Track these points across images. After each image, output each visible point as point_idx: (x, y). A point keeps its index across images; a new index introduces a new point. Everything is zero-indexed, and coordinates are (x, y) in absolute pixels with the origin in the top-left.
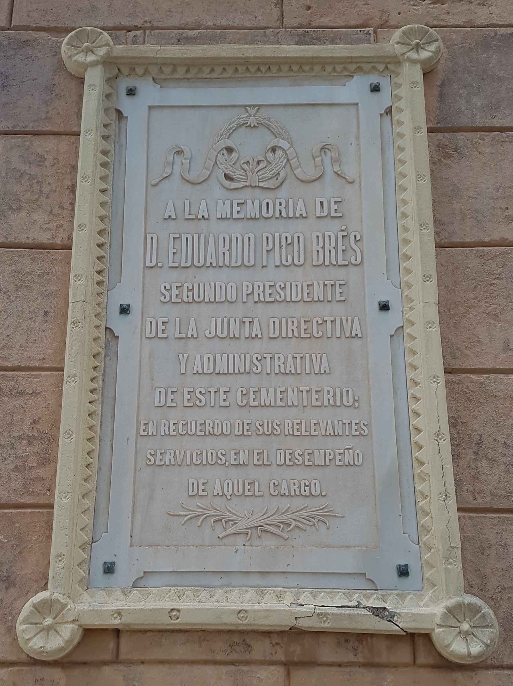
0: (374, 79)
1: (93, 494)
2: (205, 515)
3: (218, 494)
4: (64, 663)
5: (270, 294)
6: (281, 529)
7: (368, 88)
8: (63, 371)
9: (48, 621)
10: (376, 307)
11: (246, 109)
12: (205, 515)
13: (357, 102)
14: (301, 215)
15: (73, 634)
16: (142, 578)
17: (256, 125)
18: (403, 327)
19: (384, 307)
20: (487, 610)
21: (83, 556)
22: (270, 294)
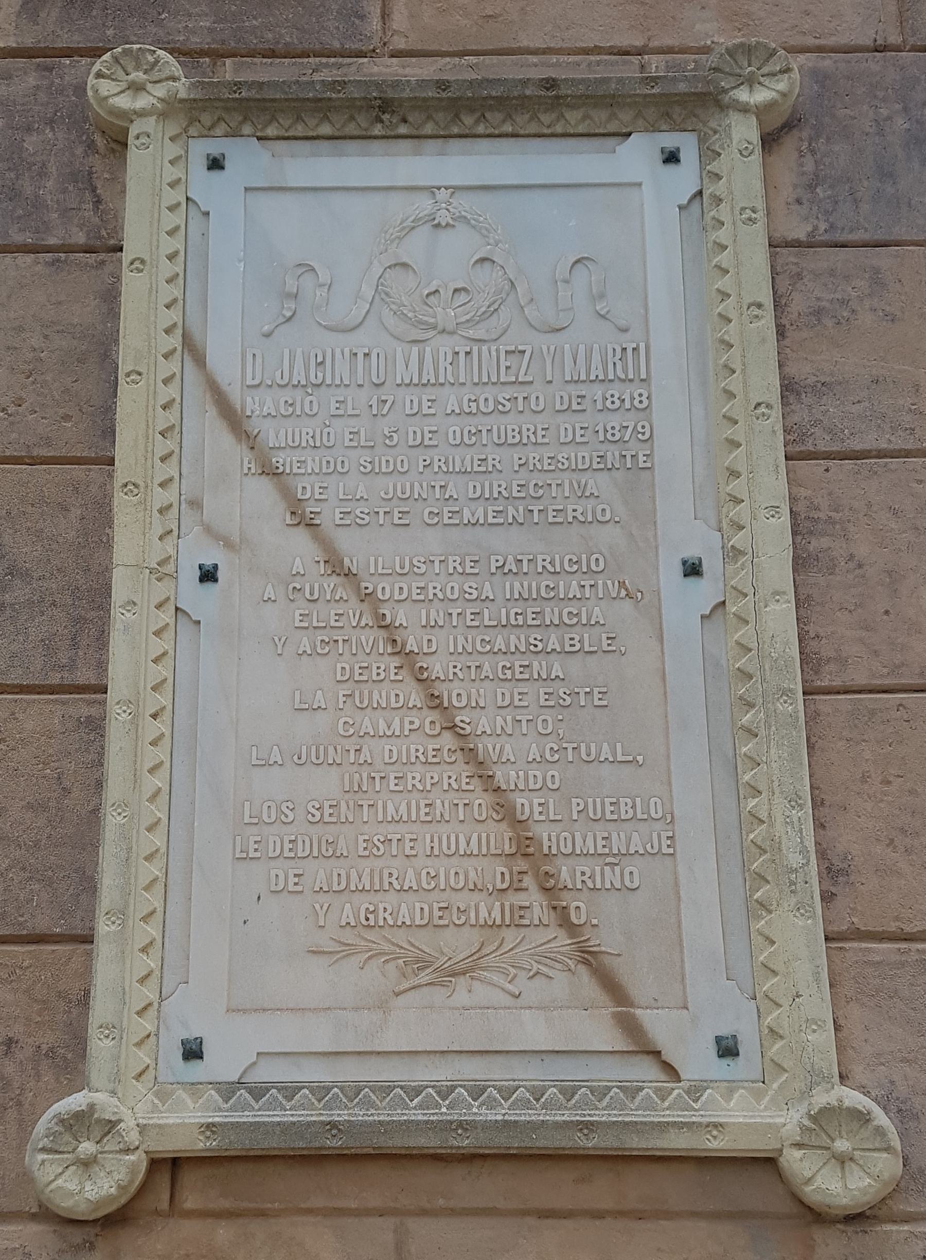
0: (670, 140)
1: (167, 740)
2: (370, 954)
3: (453, 411)
4: (116, 1219)
5: (507, 368)
6: (510, 977)
7: (658, 157)
8: (106, 693)
9: (87, 1147)
10: (679, 570)
11: (433, 193)
12: (370, 954)
13: (639, 180)
14: (500, 650)
15: (133, 1172)
16: (254, 1064)
17: (451, 222)
18: (724, 602)
19: (693, 570)
20: (881, 1118)
21: (153, 872)
22: (507, 368)
